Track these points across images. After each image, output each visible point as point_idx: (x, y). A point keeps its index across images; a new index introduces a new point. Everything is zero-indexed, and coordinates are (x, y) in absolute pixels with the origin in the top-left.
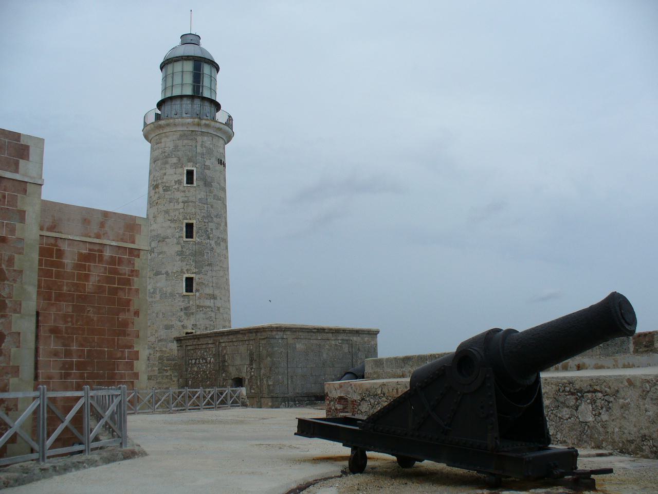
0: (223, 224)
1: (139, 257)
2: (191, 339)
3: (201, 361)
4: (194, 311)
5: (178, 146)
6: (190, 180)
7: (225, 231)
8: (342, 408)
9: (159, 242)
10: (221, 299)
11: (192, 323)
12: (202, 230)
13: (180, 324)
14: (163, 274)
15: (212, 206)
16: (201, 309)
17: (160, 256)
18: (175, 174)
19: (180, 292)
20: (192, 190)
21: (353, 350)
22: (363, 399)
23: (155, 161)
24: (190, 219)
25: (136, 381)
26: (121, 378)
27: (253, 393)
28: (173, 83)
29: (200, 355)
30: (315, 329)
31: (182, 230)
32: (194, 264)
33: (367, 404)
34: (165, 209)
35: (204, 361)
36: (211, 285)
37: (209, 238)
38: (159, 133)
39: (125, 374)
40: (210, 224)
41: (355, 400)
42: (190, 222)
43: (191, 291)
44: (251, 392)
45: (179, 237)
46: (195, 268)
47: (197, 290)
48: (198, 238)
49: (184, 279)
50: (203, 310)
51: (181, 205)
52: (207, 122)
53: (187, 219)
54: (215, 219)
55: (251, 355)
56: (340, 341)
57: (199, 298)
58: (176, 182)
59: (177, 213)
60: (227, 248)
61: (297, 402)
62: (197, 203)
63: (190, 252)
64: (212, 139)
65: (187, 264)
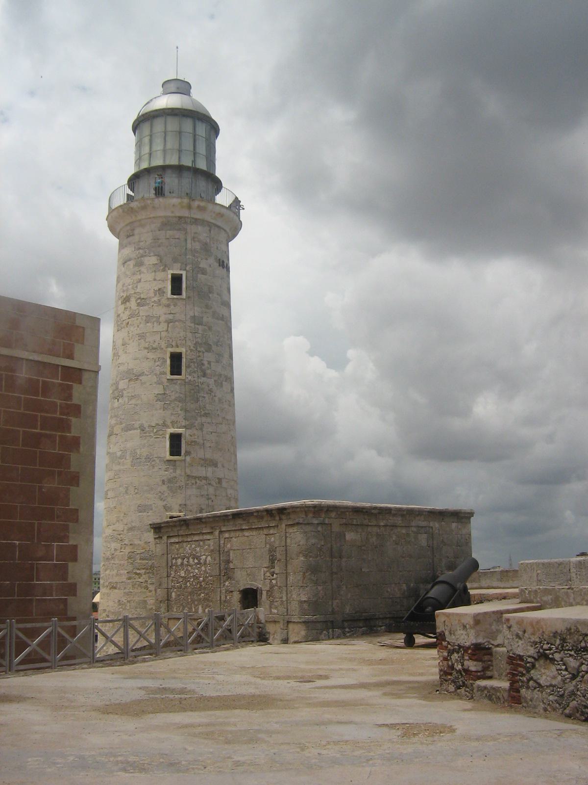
0: (226, 356)
1: (81, 383)
2: (175, 526)
3: (191, 560)
5: (158, 239)
7: (231, 365)
8: (480, 669)
10: (223, 466)
11: (180, 502)
12: (194, 362)
13: (161, 503)
14: (136, 429)
15: (210, 328)
18: (155, 280)
19: (162, 455)
21: (435, 542)
22: (543, 656)
23: (125, 262)
24: (177, 346)
25: (71, 599)
26: (45, 594)
27: (274, 614)
28: (150, 150)
29: (189, 551)
31: (165, 361)
32: (182, 413)
33: (553, 668)
34: (139, 331)
35: (196, 561)
36: (208, 444)
37: (204, 375)
39: (51, 586)
40: (206, 354)
41: (521, 658)
42: (178, 350)
43: (178, 453)
44: (271, 613)
47: (188, 453)
49: (168, 436)
50: (196, 483)
51: (164, 326)
53: (173, 347)
55: (272, 551)
56: (414, 529)
57: (191, 465)
58: (155, 292)
59: (157, 338)
60: (232, 390)
61: (347, 630)
63: (177, 395)
64: (210, 231)
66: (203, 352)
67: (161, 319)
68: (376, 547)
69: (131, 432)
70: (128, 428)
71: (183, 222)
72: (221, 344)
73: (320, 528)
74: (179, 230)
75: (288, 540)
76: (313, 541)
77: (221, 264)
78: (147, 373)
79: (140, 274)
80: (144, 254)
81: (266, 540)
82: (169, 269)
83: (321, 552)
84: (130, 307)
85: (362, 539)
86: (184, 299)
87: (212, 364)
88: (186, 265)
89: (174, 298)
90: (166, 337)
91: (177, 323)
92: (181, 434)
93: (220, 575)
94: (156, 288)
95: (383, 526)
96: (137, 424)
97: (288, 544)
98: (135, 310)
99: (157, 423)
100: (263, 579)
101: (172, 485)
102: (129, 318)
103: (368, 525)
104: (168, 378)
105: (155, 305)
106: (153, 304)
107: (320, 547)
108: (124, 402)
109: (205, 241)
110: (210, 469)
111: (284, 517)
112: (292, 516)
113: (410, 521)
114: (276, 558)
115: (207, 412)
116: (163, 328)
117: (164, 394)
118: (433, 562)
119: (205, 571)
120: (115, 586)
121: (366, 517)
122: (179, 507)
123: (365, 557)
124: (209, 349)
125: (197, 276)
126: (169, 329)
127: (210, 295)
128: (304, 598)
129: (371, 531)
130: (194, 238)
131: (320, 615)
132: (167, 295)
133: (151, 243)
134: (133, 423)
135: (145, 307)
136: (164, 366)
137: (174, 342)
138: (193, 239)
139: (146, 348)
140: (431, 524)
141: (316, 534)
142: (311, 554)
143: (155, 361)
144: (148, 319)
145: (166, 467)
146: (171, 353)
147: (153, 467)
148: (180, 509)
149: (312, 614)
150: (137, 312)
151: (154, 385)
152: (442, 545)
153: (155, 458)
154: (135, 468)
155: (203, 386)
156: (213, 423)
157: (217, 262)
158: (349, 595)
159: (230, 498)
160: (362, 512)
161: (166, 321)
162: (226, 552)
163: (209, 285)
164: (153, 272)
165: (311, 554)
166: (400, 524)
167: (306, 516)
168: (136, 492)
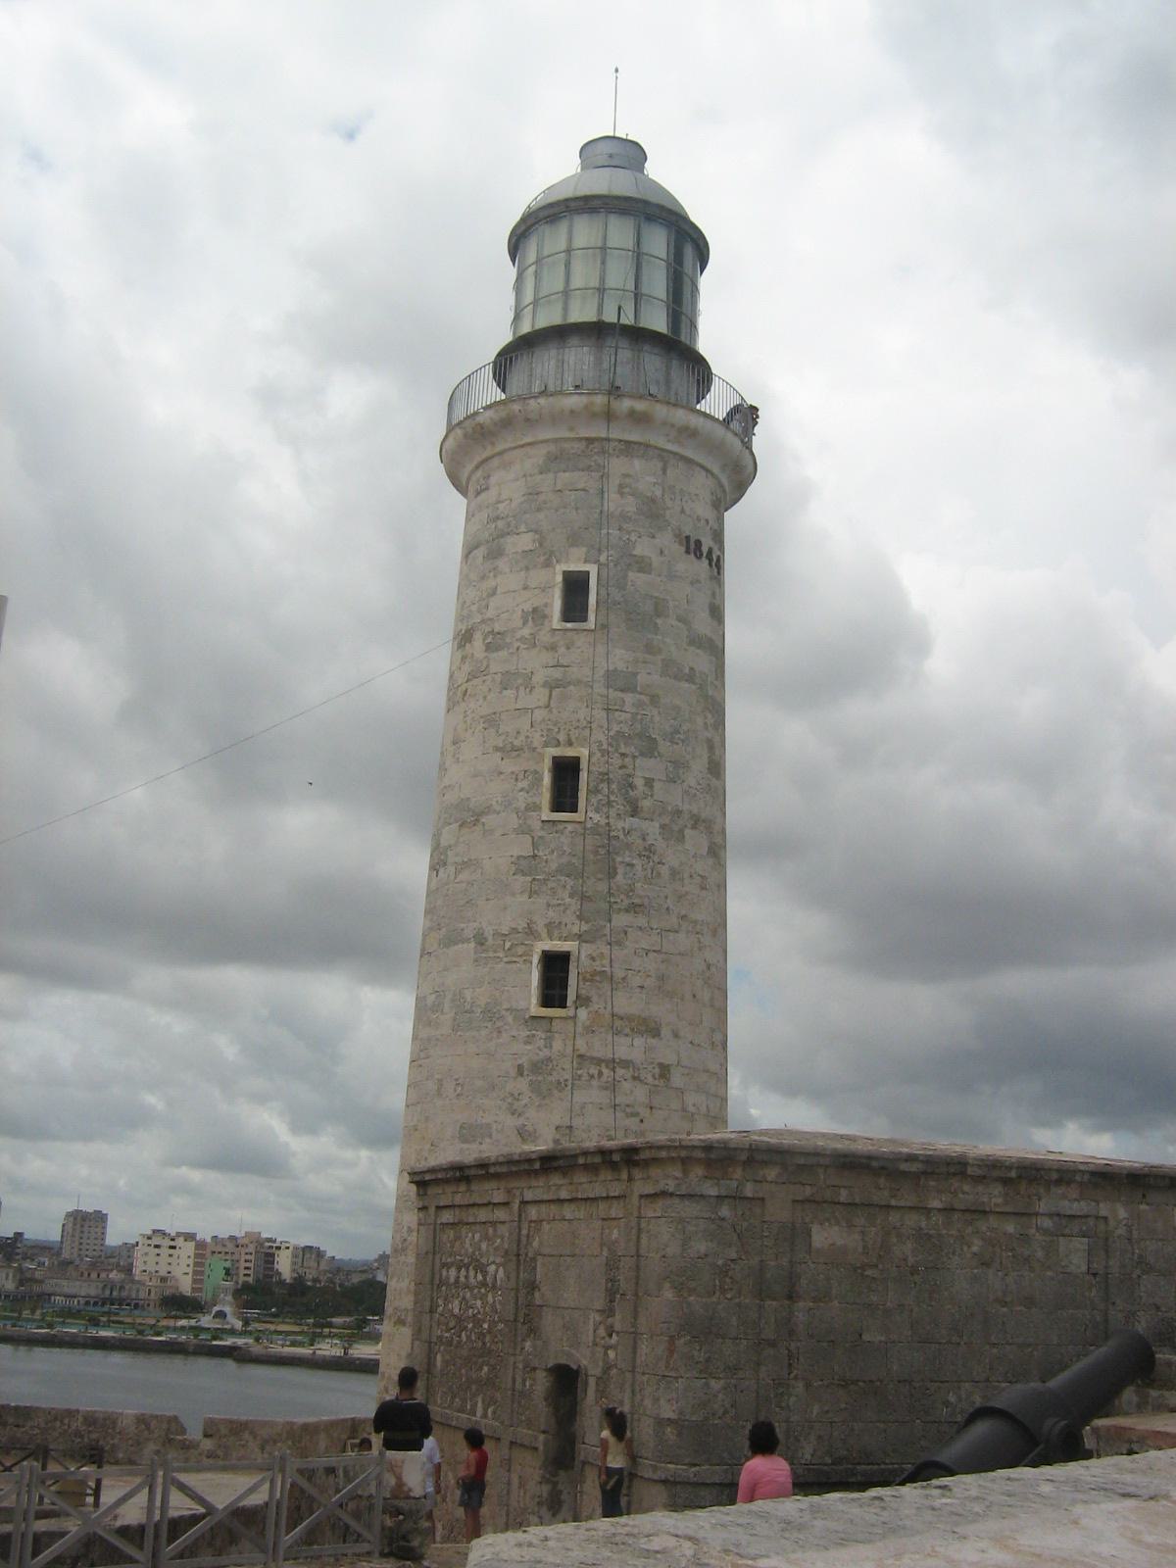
3: (472, 1273)
4: (568, 1076)
9: (461, 826)
10: (676, 1035)
12: (609, 781)
13: (511, 1122)
14: (468, 940)
15: (654, 700)
16: (594, 1071)
17: (461, 877)
18: (526, 588)
19: (522, 1005)
20: (581, 640)
23: (470, 553)
24: (570, 744)
30: (911, 1158)
32: (574, 904)
36: (636, 981)
37: (635, 812)
38: (484, 456)
42: (570, 752)
45: (528, 808)
46: (580, 918)
47: (582, 1001)
48: (597, 811)
49: (536, 959)
50: (600, 1074)
51: (540, 695)
52: (640, 406)
53: (558, 744)
57: (589, 1031)
59: (524, 723)
62: (596, 685)
63: (565, 860)
64: (664, 471)
65: (548, 905)
66: (634, 757)
67: (535, 679)
68: (914, 1271)
69: (456, 947)
70: (450, 941)
71: (596, 450)
72: (682, 737)
73: (725, 1211)
74: (588, 468)
75: (644, 1241)
76: (702, 1246)
77: (692, 546)
78: (498, 808)
79: (495, 576)
80: (506, 530)
81: (602, 1234)
83: (728, 1280)
84: (473, 654)
85: (865, 1247)
86: (592, 631)
87: (657, 785)
88: (600, 550)
89: (566, 630)
90: (544, 720)
91: (572, 687)
92: (569, 952)
93: (515, 1320)
94: (528, 607)
95: (939, 1210)
96: (469, 933)
97: (642, 1252)
98: (481, 661)
99: (513, 926)
100: (590, 1344)
101: (540, 1078)
102: (467, 682)
103: (888, 1207)
104: (545, 818)
106: (519, 644)
107: (725, 1265)
108: (449, 876)
109: (649, 494)
110: (639, 1041)
111: (637, 1173)
112: (655, 1171)
113: (1029, 1197)
114: (618, 1289)
116: (539, 700)
117: (535, 856)
118: (1106, 1321)
119: (493, 1306)
120: (403, 1317)
121: (882, 1181)
122: (554, 1131)
123: (874, 1298)
124: (650, 749)
125: (625, 577)
126: (552, 702)
127: (659, 621)
128: (668, 1412)
129: (898, 1224)
130: (621, 486)
131: (711, 1465)
132: (550, 621)
133: (522, 503)
134: (462, 925)
135: (500, 653)
136: (537, 790)
137: (562, 732)
138: (621, 490)
139: (497, 749)
140: (1104, 1209)
141: (713, 1226)
142: (692, 1284)
143: (517, 780)
144: (507, 681)
146: (554, 758)
147: (500, 1032)
148: (558, 1137)
149: (687, 1461)
150: (485, 665)
151: (513, 836)
152: (1138, 1272)
153: (504, 1012)
154: (459, 1033)
155: (630, 839)
156: (652, 929)
157: (681, 544)
158: (816, 1410)
159: (693, 1115)
160: (868, 1167)
161: (546, 684)
162: (531, 1259)
163: (656, 598)
164: (521, 570)
165: (692, 1284)
166: (996, 1205)
167: (685, 1172)
168: (458, 1091)
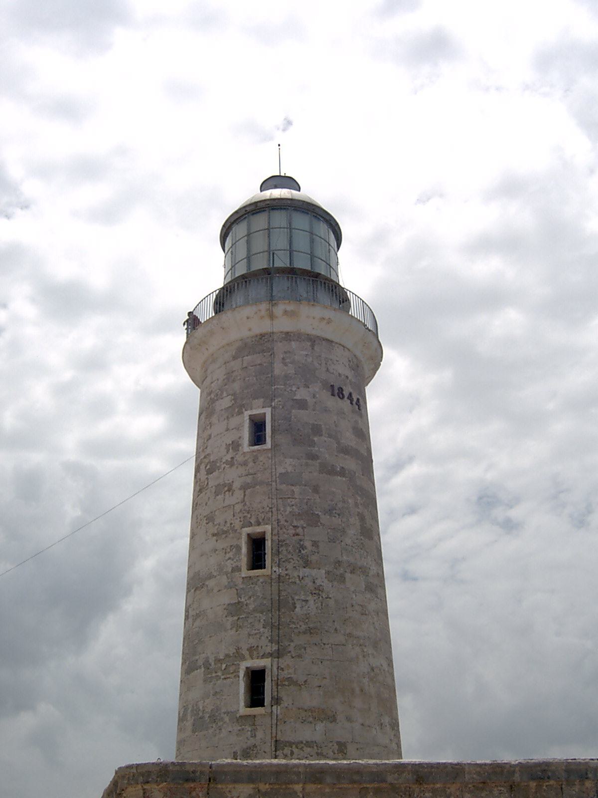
6: (258, 435)
15: (316, 489)
24: (259, 524)
28: (249, 250)
37: (307, 564)
42: (259, 529)
45: (233, 570)
47: (277, 701)
49: (242, 674)
53: (250, 525)
54: (325, 519)
58: (228, 446)
82: (246, 410)
105: (227, 466)
110: (320, 727)
115: (311, 626)
117: (239, 602)
139: (214, 535)
143: (226, 553)
145: (240, 728)
